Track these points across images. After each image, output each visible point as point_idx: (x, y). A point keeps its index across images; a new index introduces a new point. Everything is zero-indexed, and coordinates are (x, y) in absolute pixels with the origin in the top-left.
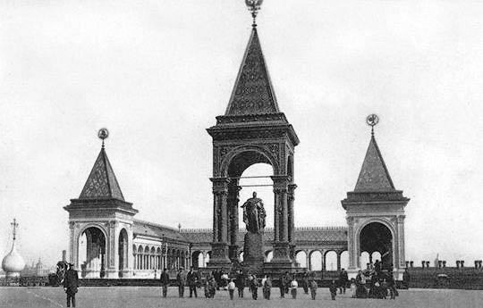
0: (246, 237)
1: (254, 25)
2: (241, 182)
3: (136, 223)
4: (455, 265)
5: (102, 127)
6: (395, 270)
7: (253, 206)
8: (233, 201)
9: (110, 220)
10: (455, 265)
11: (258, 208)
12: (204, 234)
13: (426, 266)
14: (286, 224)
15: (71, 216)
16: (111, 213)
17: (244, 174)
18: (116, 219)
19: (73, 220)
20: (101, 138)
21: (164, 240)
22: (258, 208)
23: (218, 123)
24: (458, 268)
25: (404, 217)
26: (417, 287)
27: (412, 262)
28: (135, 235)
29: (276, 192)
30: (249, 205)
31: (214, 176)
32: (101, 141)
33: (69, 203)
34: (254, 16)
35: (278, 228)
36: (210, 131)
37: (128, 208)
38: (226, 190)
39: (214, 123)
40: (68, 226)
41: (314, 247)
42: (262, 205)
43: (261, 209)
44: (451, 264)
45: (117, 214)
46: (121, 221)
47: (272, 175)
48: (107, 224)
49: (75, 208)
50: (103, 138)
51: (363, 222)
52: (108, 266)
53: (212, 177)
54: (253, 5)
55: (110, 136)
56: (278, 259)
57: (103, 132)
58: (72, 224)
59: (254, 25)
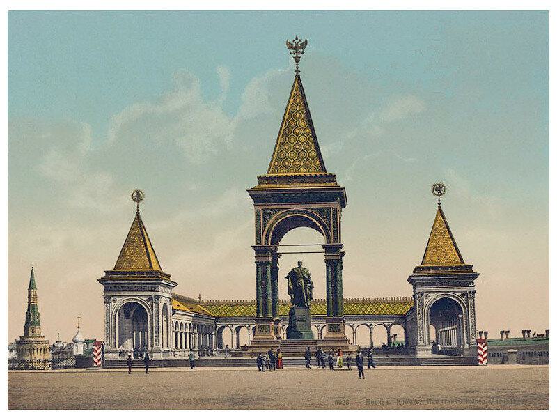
0: (291, 312)
1: (297, 71)
2: (280, 250)
3: (176, 297)
4: (521, 336)
5: (444, 182)
6: (150, 349)
7: (299, 279)
8: (275, 270)
9: (468, 289)
10: (521, 336)
11: (304, 278)
12: (246, 304)
13: (483, 337)
14: (270, 298)
15: (106, 290)
16: (153, 287)
17: (280, 243)
18: (160, 294)
19: (109, 294)
20: (135, 200)
21: (196, 316)
22: (304, 278)
23: (260, 183)
24: (502, 339)
25: (474, 292)
26: (399, 365)
27: (486, 333)
28: (174, 311)
29: (258, 263)
30: (293, 276)
31: (257, 243)
32: (299, 69)
33: (103, 275)
34: (297, 60)
35: (261, 299)
36: (254, 194)
37: (171, 285)
38: (270, 259)
39: (254, 184)
40: (103, 300)
41: (240, 324)
42: (309, 275)
43: (308, 280)
44: (516, 334)
45: (161, 288)
46: (164, 293)
47: (324, 243)
48: (465, 294)
49: (111, 282)
50: (440, 194)
51: (120, 302)
52: (152, 346)
53: (254, 245)
54: (295, 48)
55: (145, 198)
56: (331, 335)
57: (138, 194)
58: (107, 299)
59: (297, 71)
